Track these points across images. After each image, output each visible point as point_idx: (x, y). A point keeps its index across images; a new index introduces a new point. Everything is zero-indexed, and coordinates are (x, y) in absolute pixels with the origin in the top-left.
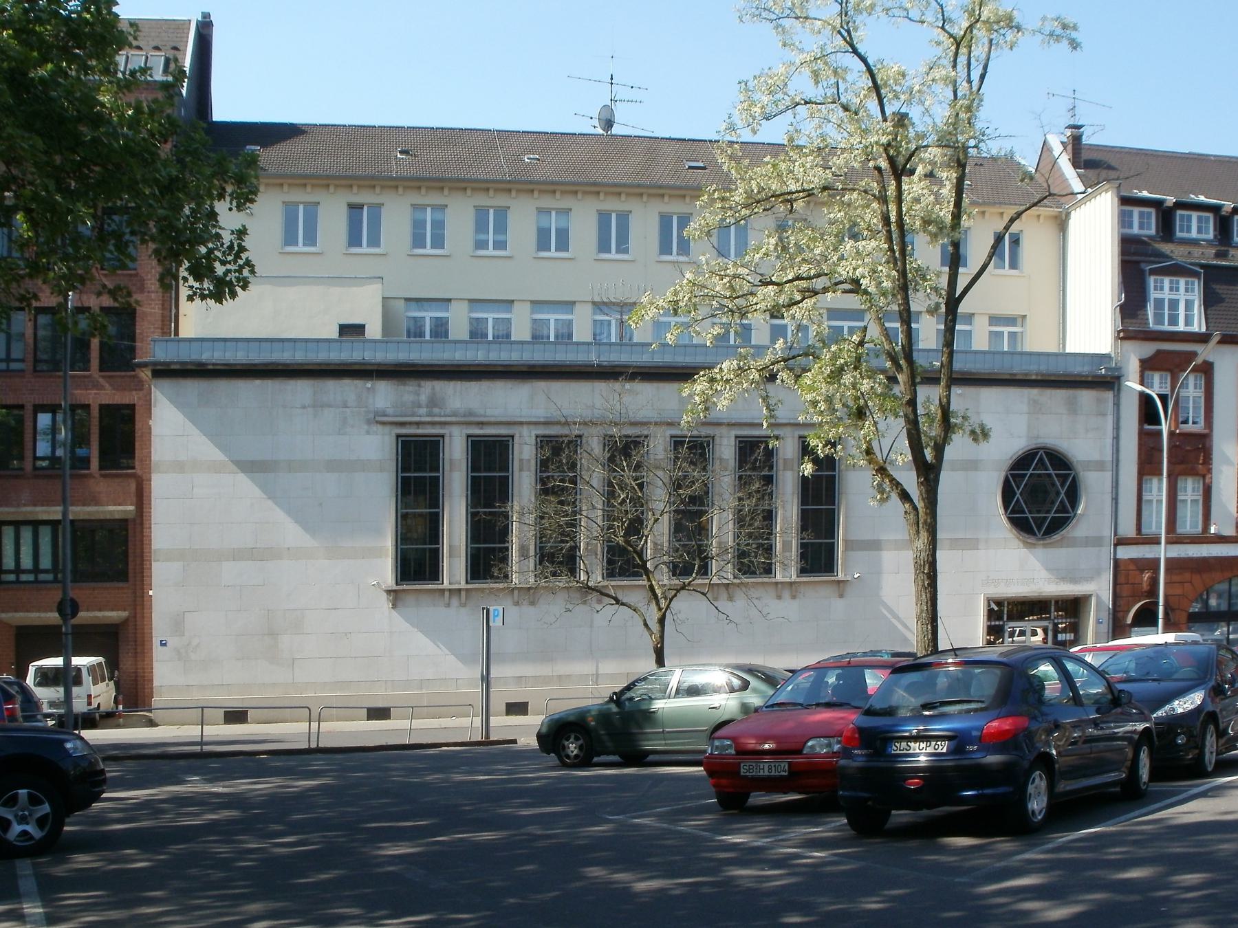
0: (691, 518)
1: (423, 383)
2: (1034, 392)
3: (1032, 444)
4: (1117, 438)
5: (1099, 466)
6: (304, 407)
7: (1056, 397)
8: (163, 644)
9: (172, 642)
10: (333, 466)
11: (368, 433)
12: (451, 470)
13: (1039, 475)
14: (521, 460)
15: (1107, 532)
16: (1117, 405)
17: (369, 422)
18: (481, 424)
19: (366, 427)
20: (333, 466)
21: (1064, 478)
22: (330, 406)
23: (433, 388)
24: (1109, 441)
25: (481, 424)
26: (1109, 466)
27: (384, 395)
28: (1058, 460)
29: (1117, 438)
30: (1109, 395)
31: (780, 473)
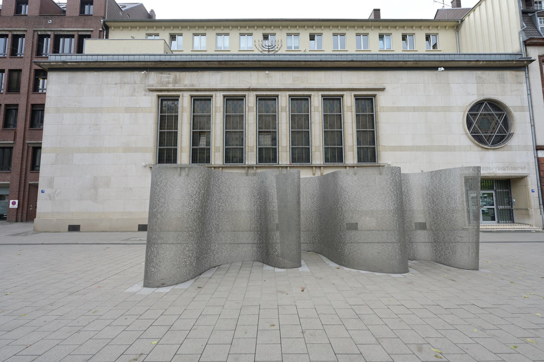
0: (268, 127)
1: (171, 73)
2: (479, 73)
3: (482, 98)
4: (530, 95)
5: (521, 109)
6: (116, 84)
7: (493, 75)
8: (43, 192)
9: (47, 191)
10: (128, 110)
11: (145, 95)
12: (181, 152)
13: (485, 115)
14: (352, 112)
15: (530, 143)
16: (528, 77)
17: (145, 91)
18: (197, 90)
19: (144, 92)
20: (128, 110)
21: (500, 116)
22: (128, 83)
23: (176, 76)
24: (525, 97)
25: (197, 90)
26: (527, 109)
27: (155, 79)
28: (495, 106)
29: (530, 95)
30: (522, 74)
31: (313, 113)
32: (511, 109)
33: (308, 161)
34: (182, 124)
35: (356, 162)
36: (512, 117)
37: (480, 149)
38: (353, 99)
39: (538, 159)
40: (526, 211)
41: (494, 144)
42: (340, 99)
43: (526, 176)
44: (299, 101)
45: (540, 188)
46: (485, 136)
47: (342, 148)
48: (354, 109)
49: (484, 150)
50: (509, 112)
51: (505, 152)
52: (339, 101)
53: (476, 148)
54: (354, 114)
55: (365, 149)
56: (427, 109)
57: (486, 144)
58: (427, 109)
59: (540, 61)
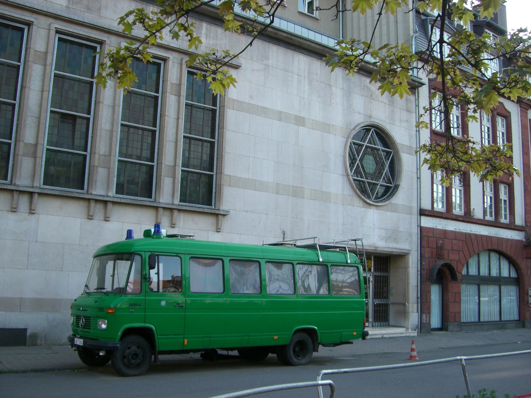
32: (399, 147)
33: (209, 203)
34: (178, 119)
35: (39, 181)
36: (399, 159)
37: (361, 203)
38: (55, 39)
39: (421, 227)
40: (404, 313)
41: (378, 198)
42: (22, 30)
43: (405, 255)
44: (75, 48)
45: (419, 273)
46: (368, 182)
47: (85, 156)
48: (52, 58)
49: (366, 205)
50: (397, 152)
51: (389, 213)
52: (19, 34)
53: (357, 202)
54: (52, 71)
55: (195, 177)
56: (300, 121)
57: (369, 197)
58: (300, 121)
59: (429, 86)
